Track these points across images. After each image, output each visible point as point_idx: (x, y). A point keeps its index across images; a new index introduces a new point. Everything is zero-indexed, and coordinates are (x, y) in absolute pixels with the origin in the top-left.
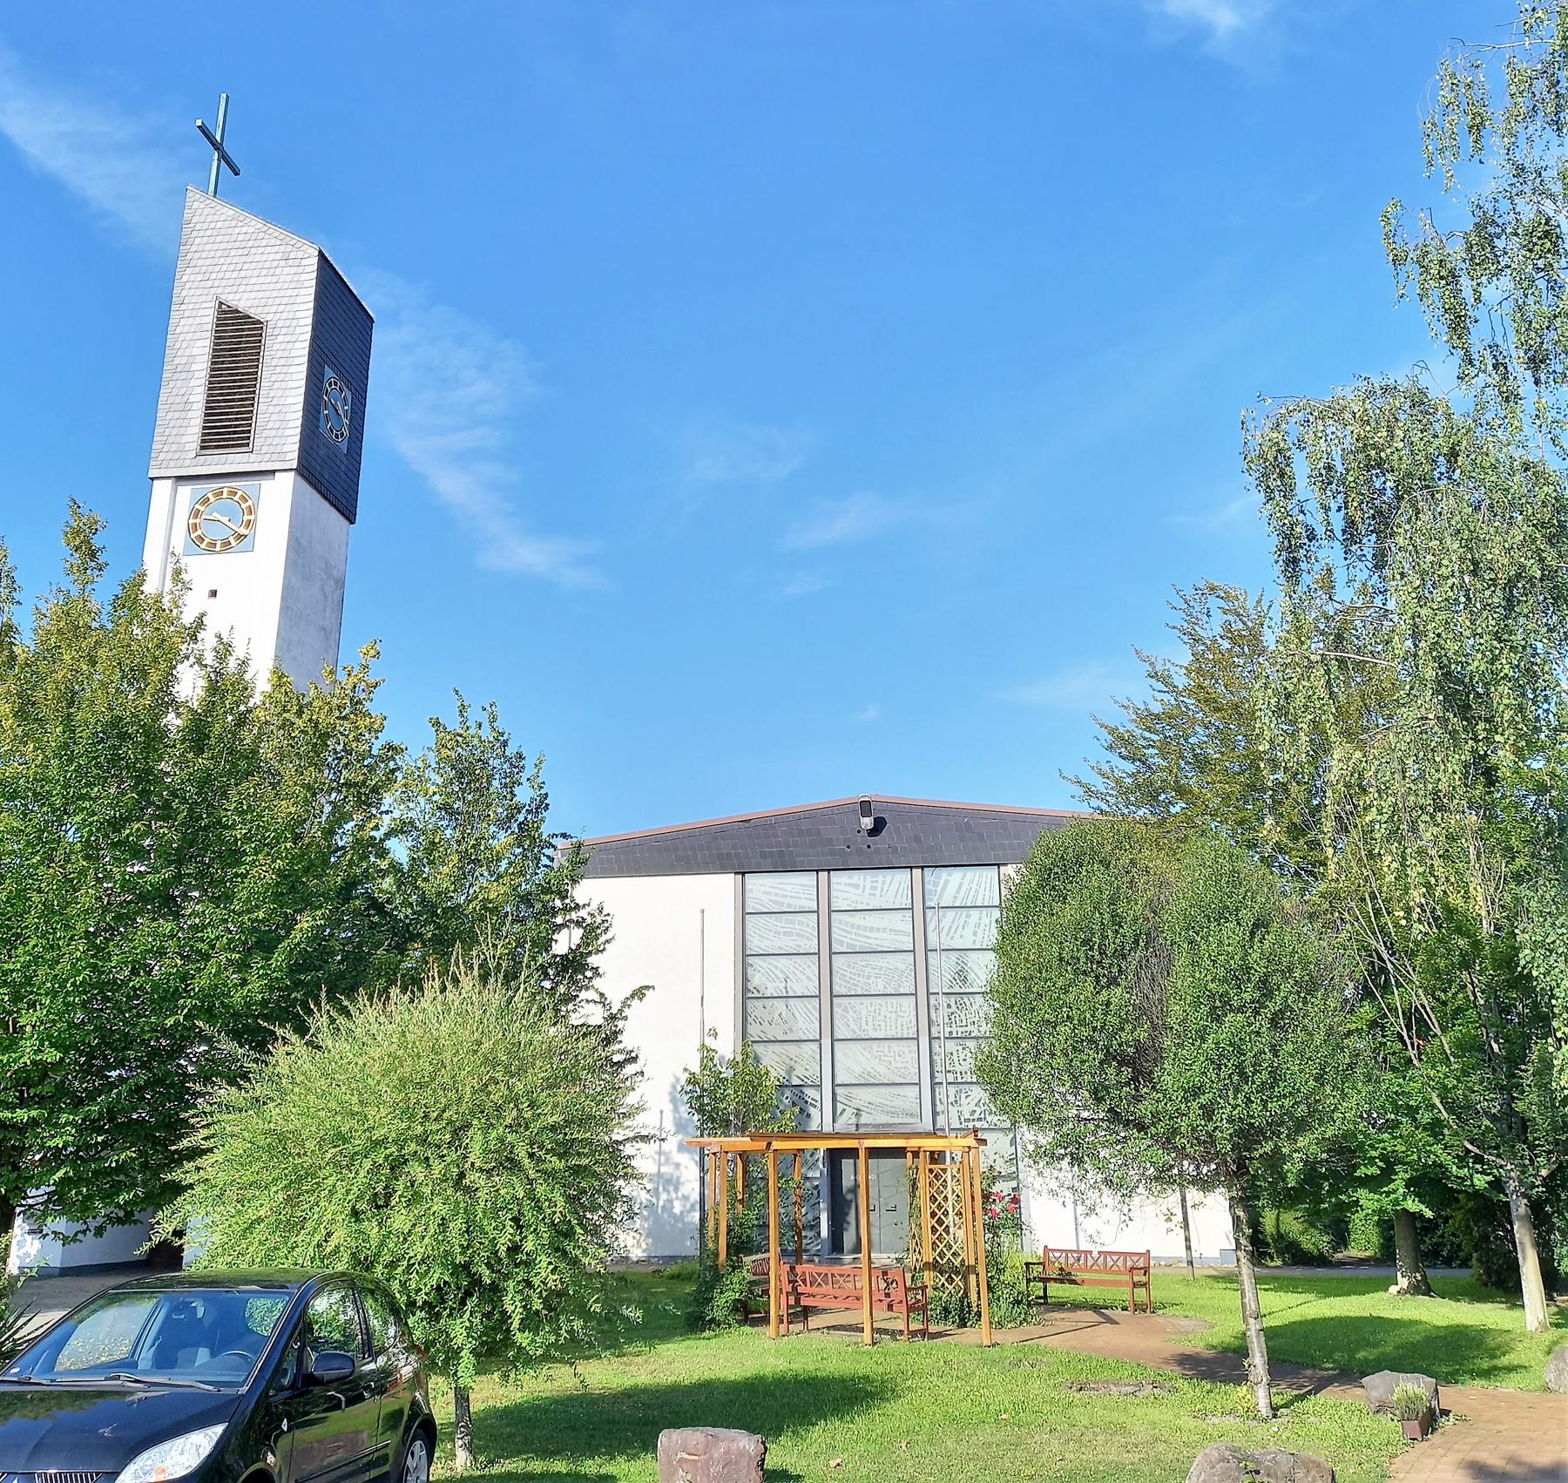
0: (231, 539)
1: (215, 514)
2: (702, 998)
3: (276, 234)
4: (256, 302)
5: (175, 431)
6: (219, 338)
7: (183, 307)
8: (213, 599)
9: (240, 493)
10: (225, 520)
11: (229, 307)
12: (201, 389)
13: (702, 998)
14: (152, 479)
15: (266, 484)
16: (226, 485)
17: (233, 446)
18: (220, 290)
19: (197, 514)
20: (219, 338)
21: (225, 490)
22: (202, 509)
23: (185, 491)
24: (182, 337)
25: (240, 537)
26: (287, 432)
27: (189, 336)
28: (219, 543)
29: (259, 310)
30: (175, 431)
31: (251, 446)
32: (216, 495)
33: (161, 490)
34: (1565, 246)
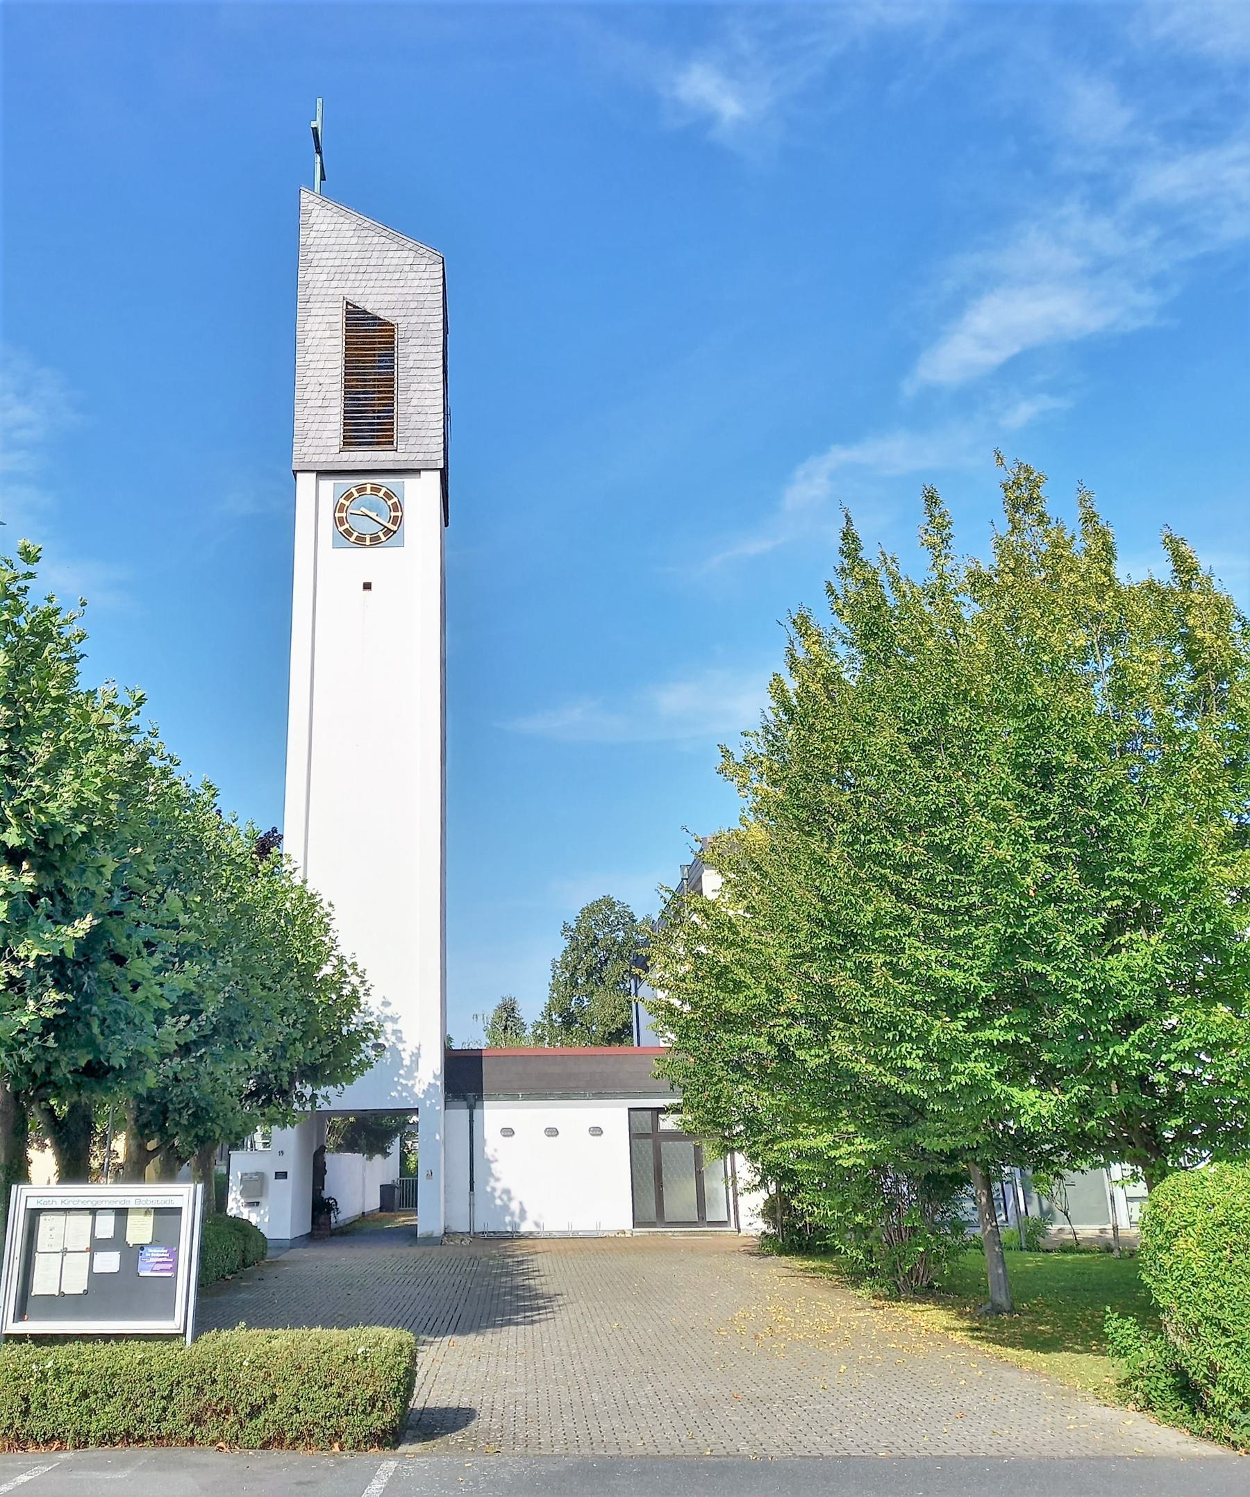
0: (381, 534)
1: (363, 509)
2: (472, 1189)
3: (366, 225)
4: (384, 305)
5: (315, 426)
6: (351, 337)
7: (309, 305)
8: (367, 592)
9: (384, 490)
10: (373, 515)
11: (355, 307)
12: (338, 386)
13: (472, 1189)
14: (295, 472)
15: (409, 483)
16: (369, 481)
17: (378, 443)
18: (346, 291)
19: (341, 508)
20: (351, 337)
21: (369, 487)
22: (347, 503)
23: (328, 485)
24: (311, 335)
25: (388, 531)
26: (430, 433)
27: (319, 334)
28: (368, 537)
29: (389, 313)
30: (315, 426)
31: (395, 444)
32: (359, 491)
33: (306, 482)
34: (1145, 1420)
